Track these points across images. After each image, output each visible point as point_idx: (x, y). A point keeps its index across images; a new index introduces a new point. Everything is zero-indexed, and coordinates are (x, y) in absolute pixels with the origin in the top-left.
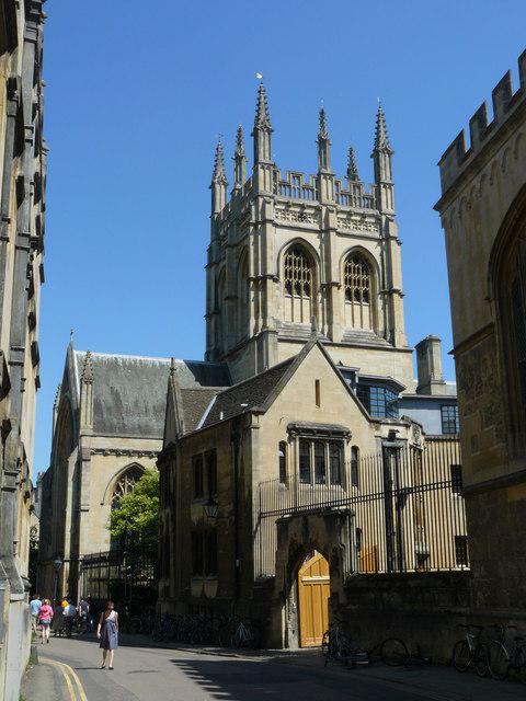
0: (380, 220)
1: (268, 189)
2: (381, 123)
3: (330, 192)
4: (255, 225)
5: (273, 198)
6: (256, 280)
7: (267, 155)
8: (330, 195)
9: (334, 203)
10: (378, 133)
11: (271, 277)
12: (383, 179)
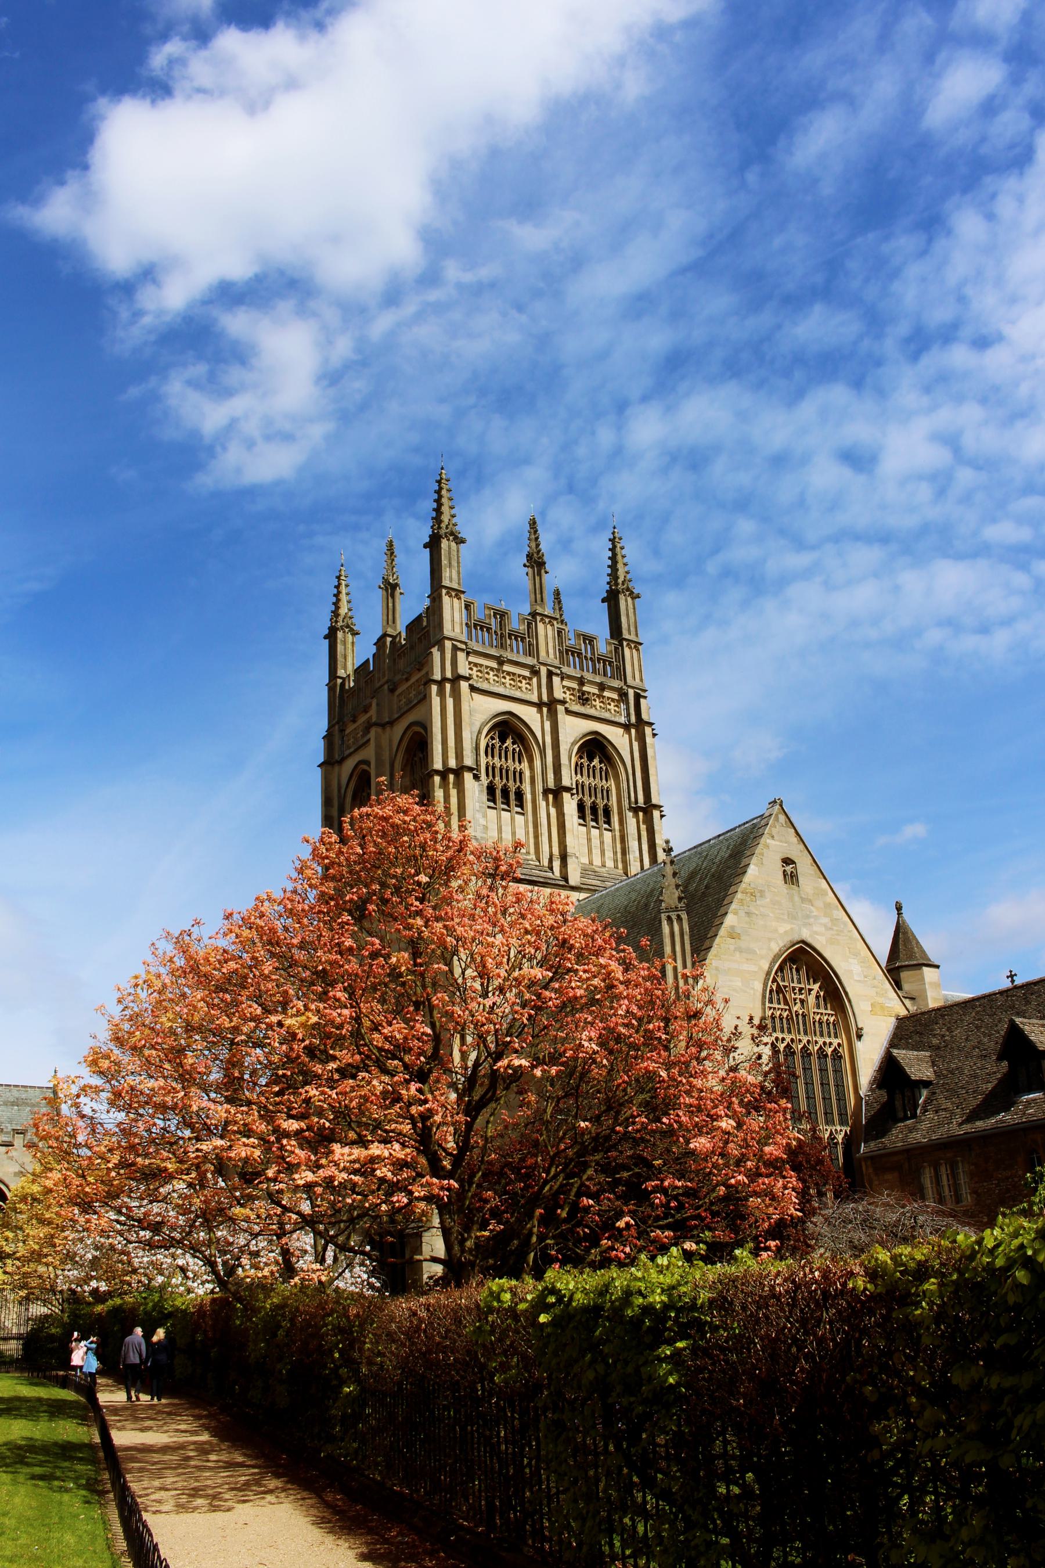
0: (626, 695)
1: (551, 656)
2: (444, 492)
3: (551, 645)
4: (441, 683)
5: (559, 668)
6: (444, 774)
7: (632, 629)
8: (551, 651)
9: (557, 663)
10: (439, 501)
11: (470, 769)
12: (446, 582)
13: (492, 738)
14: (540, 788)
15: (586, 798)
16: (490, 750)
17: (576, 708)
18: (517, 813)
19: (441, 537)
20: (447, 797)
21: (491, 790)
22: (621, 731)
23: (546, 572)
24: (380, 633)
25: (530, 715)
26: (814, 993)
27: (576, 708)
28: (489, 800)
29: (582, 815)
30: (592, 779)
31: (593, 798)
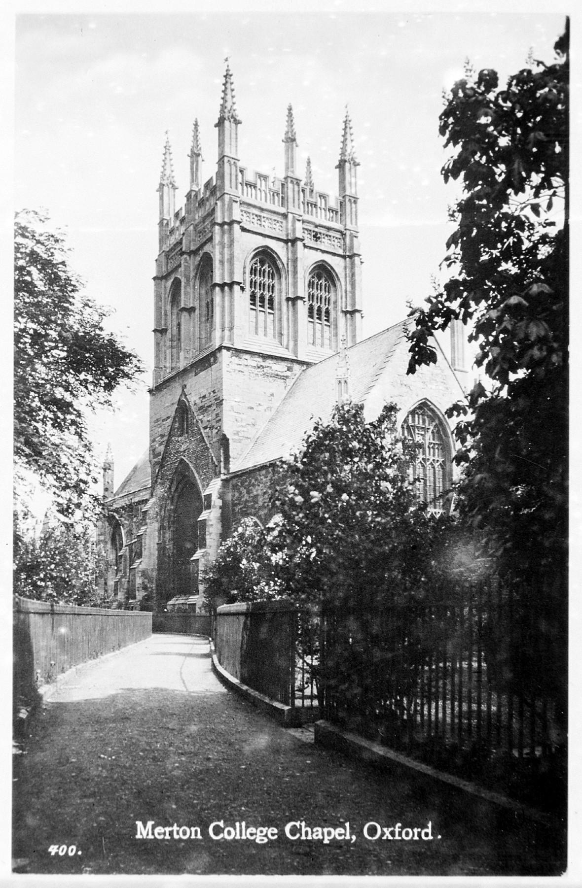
11: (239, 283)
13: (313, 277)
14: (284, 298)
15: (314, 303)
16: (253, 271)
17: (312, 243)
18: (260, 311)
19: (225, 119)
20: (223, 301)
21: (253, 297)
22: (282, 244)
23: (297, 146)
24: (189, 190)
25: (279, 249)
26: (430, 431)
27: (312, 243)
28: (251, 304)
29: (311, 315)
30: (319, 291)
31: (262, 291)
